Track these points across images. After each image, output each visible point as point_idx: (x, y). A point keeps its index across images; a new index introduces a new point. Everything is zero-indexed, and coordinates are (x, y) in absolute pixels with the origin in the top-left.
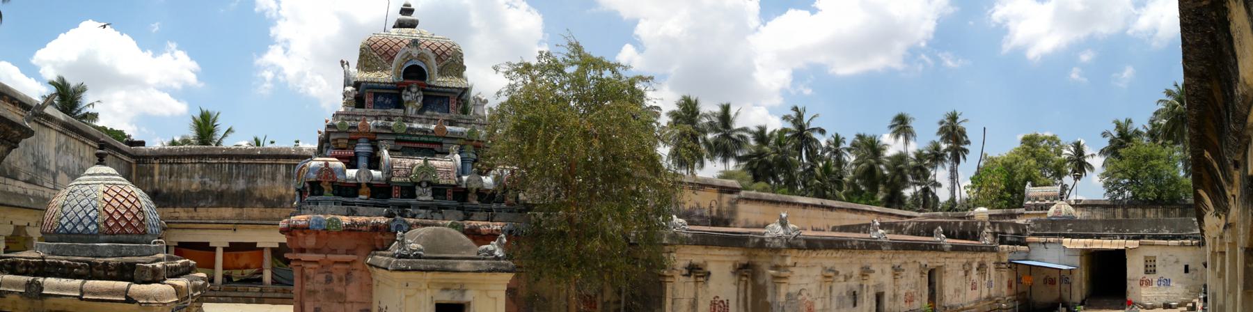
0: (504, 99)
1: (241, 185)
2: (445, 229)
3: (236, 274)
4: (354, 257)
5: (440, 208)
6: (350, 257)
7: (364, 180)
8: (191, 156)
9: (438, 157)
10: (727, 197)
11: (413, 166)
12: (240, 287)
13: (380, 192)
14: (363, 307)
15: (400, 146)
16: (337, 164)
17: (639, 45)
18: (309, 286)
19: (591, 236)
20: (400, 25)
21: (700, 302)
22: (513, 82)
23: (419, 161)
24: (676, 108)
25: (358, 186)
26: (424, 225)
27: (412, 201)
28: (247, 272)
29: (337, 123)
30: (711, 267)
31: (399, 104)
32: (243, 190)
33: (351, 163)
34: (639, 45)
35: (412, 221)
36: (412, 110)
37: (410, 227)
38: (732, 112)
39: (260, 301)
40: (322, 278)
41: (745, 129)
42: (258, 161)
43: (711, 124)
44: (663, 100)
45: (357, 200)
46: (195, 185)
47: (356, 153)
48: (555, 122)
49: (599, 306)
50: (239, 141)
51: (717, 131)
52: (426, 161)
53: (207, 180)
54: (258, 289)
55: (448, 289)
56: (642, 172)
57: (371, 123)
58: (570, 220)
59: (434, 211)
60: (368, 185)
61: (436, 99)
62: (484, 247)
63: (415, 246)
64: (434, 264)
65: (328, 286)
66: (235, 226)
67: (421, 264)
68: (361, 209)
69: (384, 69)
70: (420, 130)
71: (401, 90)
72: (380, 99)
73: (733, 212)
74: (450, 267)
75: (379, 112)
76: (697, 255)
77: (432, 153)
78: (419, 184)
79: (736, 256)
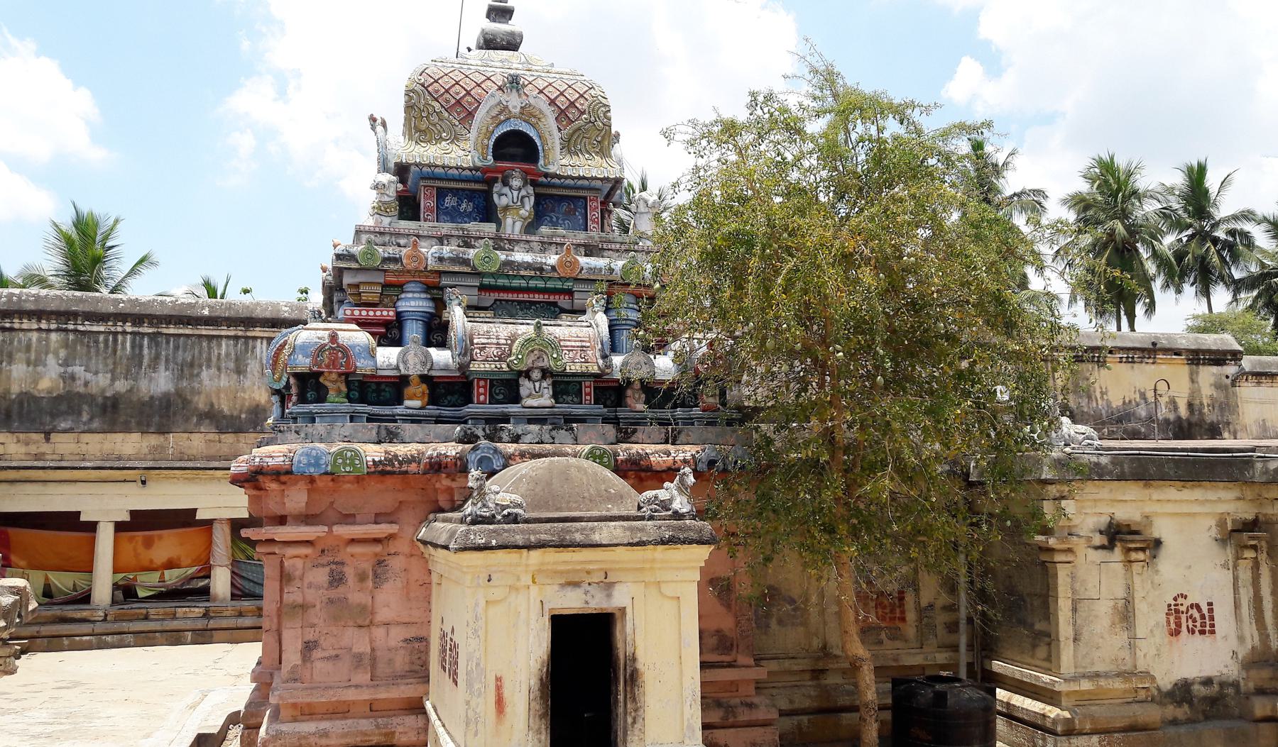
0: (684, 198)
1: (161, 382)
3: (147, 582)
4: (393, 529)
5: (569, 420)
7: (414, 368)
8: (38, 315)
9: (565, 319)
10: (1208, 374)
11: (513, 338)
12: (156, 609)
13: (449, 392)
14: (412, 632)
15: (489, 298)
16: (356, 337)
17: (993, 63)
19: (872, 469)
21: (1141, 607)
22: (701, 162)
23: (525, 329)
24: (1084, 187)
25: (403, 381)
26: (535, 456)
27: (513, 409)
28: (172, 577)
29: (357, 250)
30: (1162, 529)
31: (488, 212)
32: (166, 395)
33: (390, 333)
34: (993, 63)
35: (511, 448)
36: (512, 226)
37: (508, 461)
38: (1212, 182)
39: (203, 636)
41: (1247, 216)
42: (204, 331)
43: (1165, 214)
44: (1049, 173)
45: (399, 410)
46: (49, 379)
47: (398, 314)
48: (781, 240)
49: (911, 616)
51: (1179, 226)
52: (538, 327)
53: (78, 370)
54: (198, 611)
55: (576, 584)
56: (976, 329)
58: (829, 437)
59: (556, 427)
60: (424, 378)
61: (559, 202)
62: (649, 494)
63: (505, 498)
64: (544, 532)
65: (333, 594)
66: (145, 473)
68: (408, 429)
69: (455, 139)
70: (528, 266)
71: (491, 182)
72: (449, 201)
73: (1227, 406)
74: (578, 537)
75: (446, 228)
76: (1129, 502)
77: (553, 311)
78: (527, 374)
79: (1225, 502)
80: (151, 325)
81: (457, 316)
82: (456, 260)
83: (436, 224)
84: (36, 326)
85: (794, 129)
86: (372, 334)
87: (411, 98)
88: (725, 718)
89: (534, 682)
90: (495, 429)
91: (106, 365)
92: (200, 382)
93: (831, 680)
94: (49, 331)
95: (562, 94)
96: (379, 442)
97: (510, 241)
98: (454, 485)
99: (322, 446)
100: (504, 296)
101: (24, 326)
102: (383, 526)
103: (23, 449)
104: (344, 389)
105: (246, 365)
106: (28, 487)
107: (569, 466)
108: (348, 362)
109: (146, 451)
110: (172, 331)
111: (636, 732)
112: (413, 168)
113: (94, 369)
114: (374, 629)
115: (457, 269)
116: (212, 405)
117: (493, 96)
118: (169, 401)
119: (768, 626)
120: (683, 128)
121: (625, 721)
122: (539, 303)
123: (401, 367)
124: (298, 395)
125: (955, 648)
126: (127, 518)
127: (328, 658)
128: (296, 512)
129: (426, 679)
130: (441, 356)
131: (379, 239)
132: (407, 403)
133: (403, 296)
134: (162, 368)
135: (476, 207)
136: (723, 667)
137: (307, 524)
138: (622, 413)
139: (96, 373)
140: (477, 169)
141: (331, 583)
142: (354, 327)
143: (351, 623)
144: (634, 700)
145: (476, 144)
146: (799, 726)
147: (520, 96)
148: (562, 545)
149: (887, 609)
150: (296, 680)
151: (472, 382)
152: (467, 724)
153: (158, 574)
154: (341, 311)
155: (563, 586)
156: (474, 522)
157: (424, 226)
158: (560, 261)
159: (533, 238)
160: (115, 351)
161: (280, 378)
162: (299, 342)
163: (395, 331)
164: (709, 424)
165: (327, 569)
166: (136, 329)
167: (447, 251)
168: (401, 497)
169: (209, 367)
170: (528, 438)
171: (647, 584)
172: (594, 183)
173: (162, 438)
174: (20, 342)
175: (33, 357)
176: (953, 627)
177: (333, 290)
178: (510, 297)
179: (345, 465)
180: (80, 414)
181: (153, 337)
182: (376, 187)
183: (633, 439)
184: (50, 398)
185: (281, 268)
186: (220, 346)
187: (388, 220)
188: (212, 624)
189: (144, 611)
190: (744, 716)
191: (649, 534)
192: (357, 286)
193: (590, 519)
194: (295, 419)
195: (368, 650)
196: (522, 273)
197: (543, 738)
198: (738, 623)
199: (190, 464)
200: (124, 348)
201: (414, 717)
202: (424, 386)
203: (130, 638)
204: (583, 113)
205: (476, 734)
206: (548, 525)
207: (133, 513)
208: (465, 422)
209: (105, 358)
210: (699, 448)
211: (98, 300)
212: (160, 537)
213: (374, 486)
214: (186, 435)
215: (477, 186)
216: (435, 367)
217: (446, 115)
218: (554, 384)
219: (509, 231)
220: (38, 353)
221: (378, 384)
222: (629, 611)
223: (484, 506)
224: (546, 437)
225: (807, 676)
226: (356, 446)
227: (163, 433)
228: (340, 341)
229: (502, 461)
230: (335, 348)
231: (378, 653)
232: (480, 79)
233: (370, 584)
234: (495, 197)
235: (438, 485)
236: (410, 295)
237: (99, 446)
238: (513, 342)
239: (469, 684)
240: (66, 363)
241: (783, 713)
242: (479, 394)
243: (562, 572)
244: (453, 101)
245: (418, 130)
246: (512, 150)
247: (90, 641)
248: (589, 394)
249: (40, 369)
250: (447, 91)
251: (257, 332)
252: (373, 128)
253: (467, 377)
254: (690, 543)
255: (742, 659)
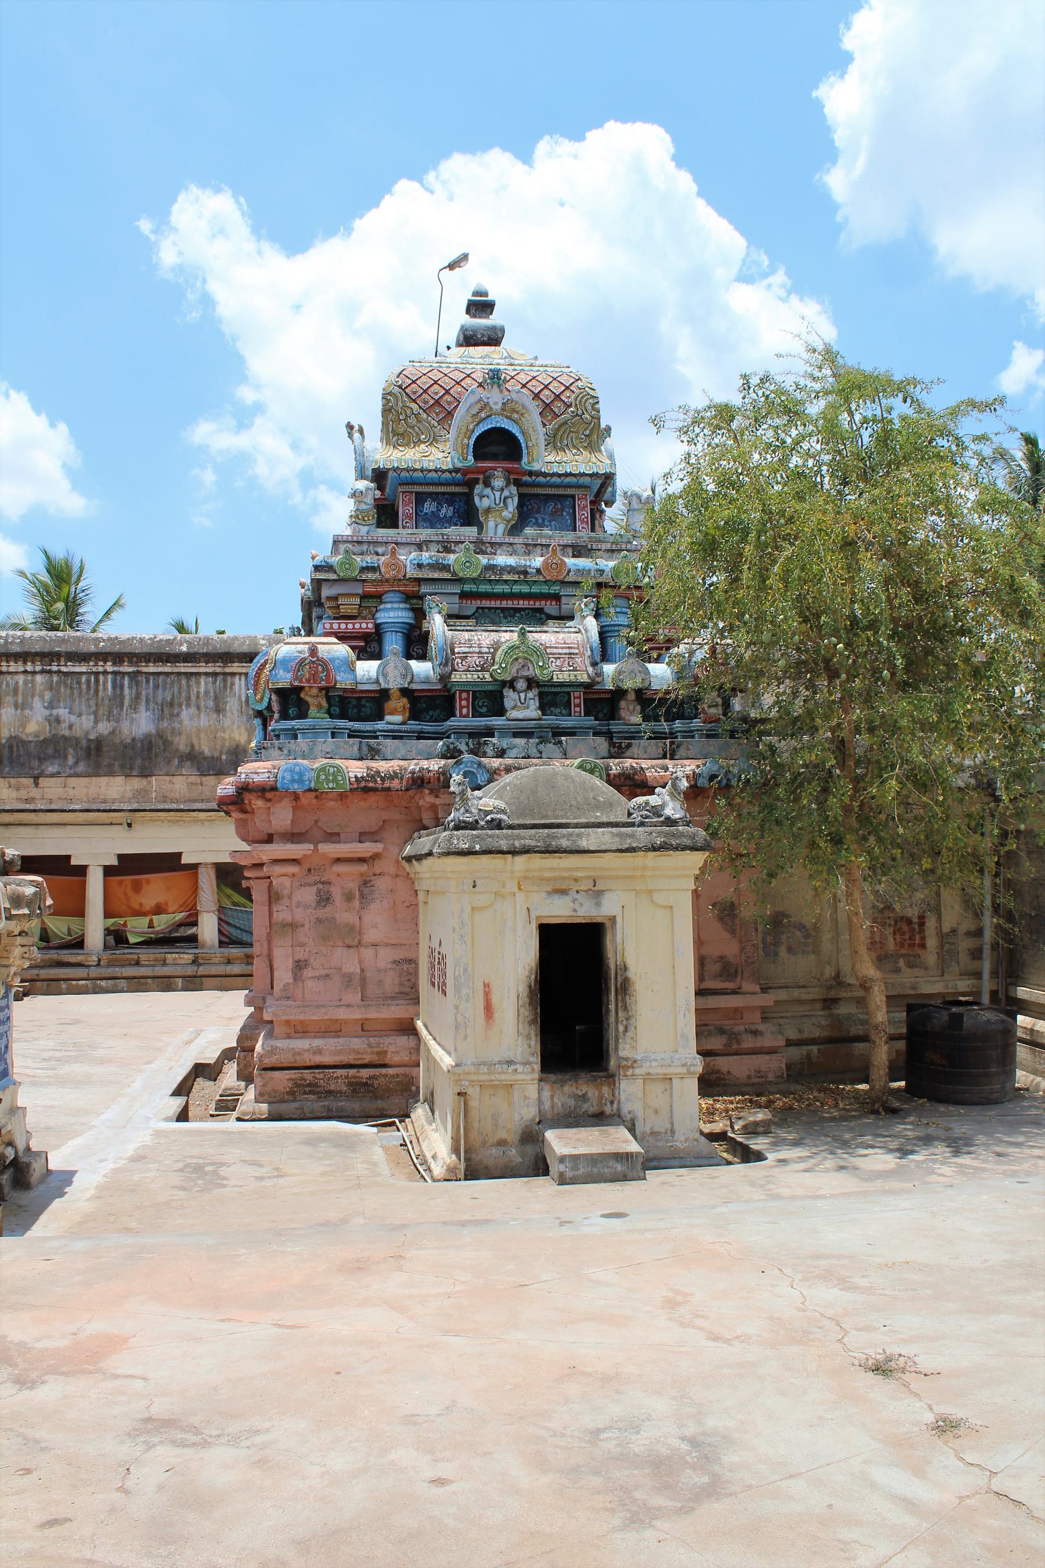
0: (676, 487)
1: (141, 723)
2: (568, 774)
3: (137, 927)
4: (378, 847)
5: (558, 733)
6: (367, 848)
7: (394, 682)
8: (24, 656)
9: (552, 626)
11: (496, 646)
12: (146, 955)
13: (430, 706)
14: (401, 954)
15: (471, 606)
18: (282, 914)
20: (469, 339)
23: (508, 636)
25: (384, 695)
27: (496, 721)
28: (162, 922)
29: (335, 560)
31: (469, 516)
33: (369, 646)
35: (496, 763)
36: (495, 528)
37: (493, 775)
39: (193, 983)
40: (308, 895)
42: (183, 667)
45: (380, 725)
46: (35, 724)
47: (378, 626)
48: (779, 528)
49: (932, 942)
50: (141, 624)
52: (523, 634)
53: (62, 712)
54: (187, 957)
55: (563, 892)
57: (408, 558)
59: (543, 740)
60: (405, 692)
61: (551, 502)
62: (641, 800)
65: (321, 913)
67: (501, 839)
69: (434, 440)
70: (511, 570)
71: (471, 484)
72: (429, 507)
74: (565, 843)
75: (425, 533)
77: (539, 617)
78: (511, 684)
80: (131, 663)
81: (437, 624)
82: (433, 567)
83: (415, 531)
84: (22, 669)
85: (792, 412)
86: (353, 648)
87: (389, 401)
88: (727, 1045)
89: (523, 989)
90: (479, 744)
91: (89, 706)
92: (181, 722)
93: (843, 1010)
94: (34, 673)
95: (546, 387)
96: (361, 759)
97: (492, 544)
98: (438, 801)
99: (305, 762)
100: (486, 603)
101: (12, 669)
102: (367, 845)
103: (14, 794)
104: (325, 704)
105: (226, 703)
106: (22, 830)
107: (555, 774)
108: (328, 676)
109: (129, 795)
110: (152, 669)
111: (628, 1040)
112: (390, 474)
113: (77, 711)
114: (362, 950)
115: (436, 576)
116: (193, 746)
117: (472, 392)
118: (150, 742)
119: (776, 954)
120: (675, 415)
121: (617, 1029)
122: (524, 609)
123: (381, 680)
124: (280, 712)
125: (978, 975)
126: (115, 862)
127: (319, 978)
128: (282, 830)
129: (416, 1001)
130: (421, 668)
131: (357, 549)
132: (388, 718)
133: (382, 607)
134: (142, 708)
135: (456, 512)
136: (727, 994)
137: (293, 842)
138: (615, 727)
139: (80, 715)
140: (456, 470)
141: (318, 902)
142: (334, 640)
143: (340, 943)
144: (626, 1009)
145: (455, 445)
146: (808, 1056)
147: (501, 391)
148: (548, 851)
149: (904, 934)
150: (288, 998)
151: (454, 695)
152: (457, 1028)
153: (145, 921)
154: (320, 626)
155: (549, 893)
156: (457, 828)
157: (402, 534)
158: (545, 563)
159: (516, 540)
160: (97, 691)
161: (262, 699)
162: (280, 655)
163: (374, 645)
164: (708, 736)
165: (314, 889)
166: (116, 669)
167: (426, 557)
168: (385, 815)
169: (188, 706)
170: (513, 753)
171: (638, 892)
172: (582, 480)
173: (144, 781)
174: (8, 685)
175: (20, 700)
176: (976, 954)
177: (313, 608)
178: (493, 604)
179: (328, 781)
180: (66, 757)
181: (134, 676)
182: (353, 495)
183: (627, 754)
184: (36, 742)
185: (261, 611)
186: (198, 683)
187: (366, 528)
188: (202, 971)
189: (135, 957)
190: (749, 1042)
191: (638, 840)
192: (335, 598)
193: (577, 826)
194: (278, 737)
195: (358, 971)
196: (505, 577)
197: (533, 1043)
198: (742, 949)
199: (174, 806)
200: (105, 689)
201: (406, 1037)
202: (405, 700)
203: (123, 983)
204: (570, 406)
205: (466, 1037)
206: (533, 831)
207: (120, 857)
208: (449, 737)
209: (88, 700)
210: (699, 762)
211: (79, 640)
212: (148, 882)
213: (357, 803)
214: (168, 778)
215: (457, 489)
216: (416, 679)
217: (425, 416)
218: (541, 695)
219: (491, 533)
220: (25, 696)
221: (359, 699)
222: (619, 920)
223: (467, 811)
224: (533, 751)
225: (819, 1005)
226: (339, 762)
227: (146, 776)
228: (320, 655)
229: (486, 776)
230: (315, 661)
231: (368, 974)
232: (459, 376)
233: (357, 903)
234: (477, 499)
235: (421, 802)
236: (389, 606)
237: (85, 791)
238: (496, 650)
239: (458, 990)
240: (51, 706)
241: (790, 1043)
242: (461, 707)
243: (548, 879)
244: (432, 402)
245: (395, 433)
246: (493, 449)
247: (87, 985)
248: (579, 706)
249: (27, 712)
250: (425, 391)
251: (235, 667)
252: (350, 436)
253: (449, 691)
254: (683, 849)
255: (747, 986)
